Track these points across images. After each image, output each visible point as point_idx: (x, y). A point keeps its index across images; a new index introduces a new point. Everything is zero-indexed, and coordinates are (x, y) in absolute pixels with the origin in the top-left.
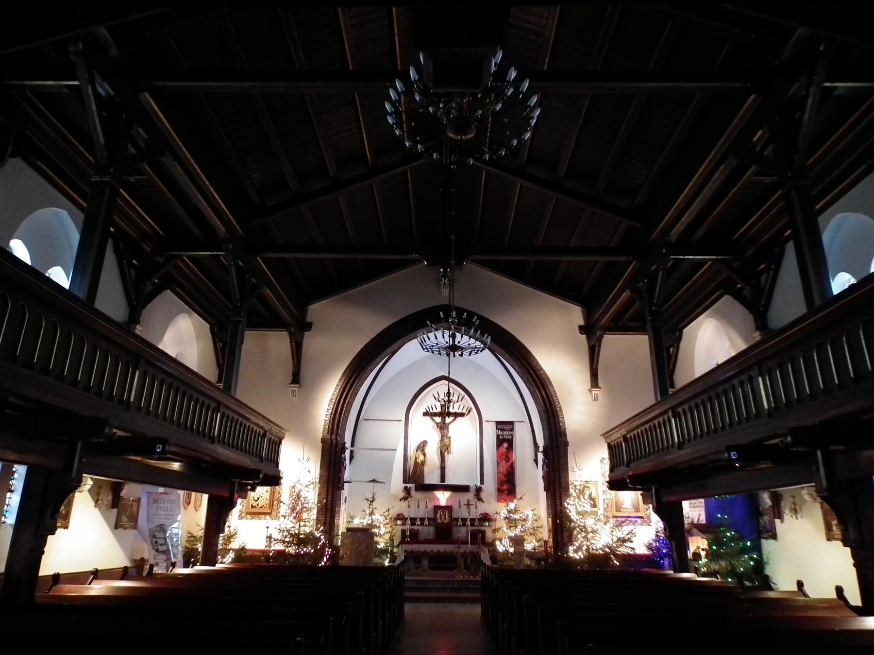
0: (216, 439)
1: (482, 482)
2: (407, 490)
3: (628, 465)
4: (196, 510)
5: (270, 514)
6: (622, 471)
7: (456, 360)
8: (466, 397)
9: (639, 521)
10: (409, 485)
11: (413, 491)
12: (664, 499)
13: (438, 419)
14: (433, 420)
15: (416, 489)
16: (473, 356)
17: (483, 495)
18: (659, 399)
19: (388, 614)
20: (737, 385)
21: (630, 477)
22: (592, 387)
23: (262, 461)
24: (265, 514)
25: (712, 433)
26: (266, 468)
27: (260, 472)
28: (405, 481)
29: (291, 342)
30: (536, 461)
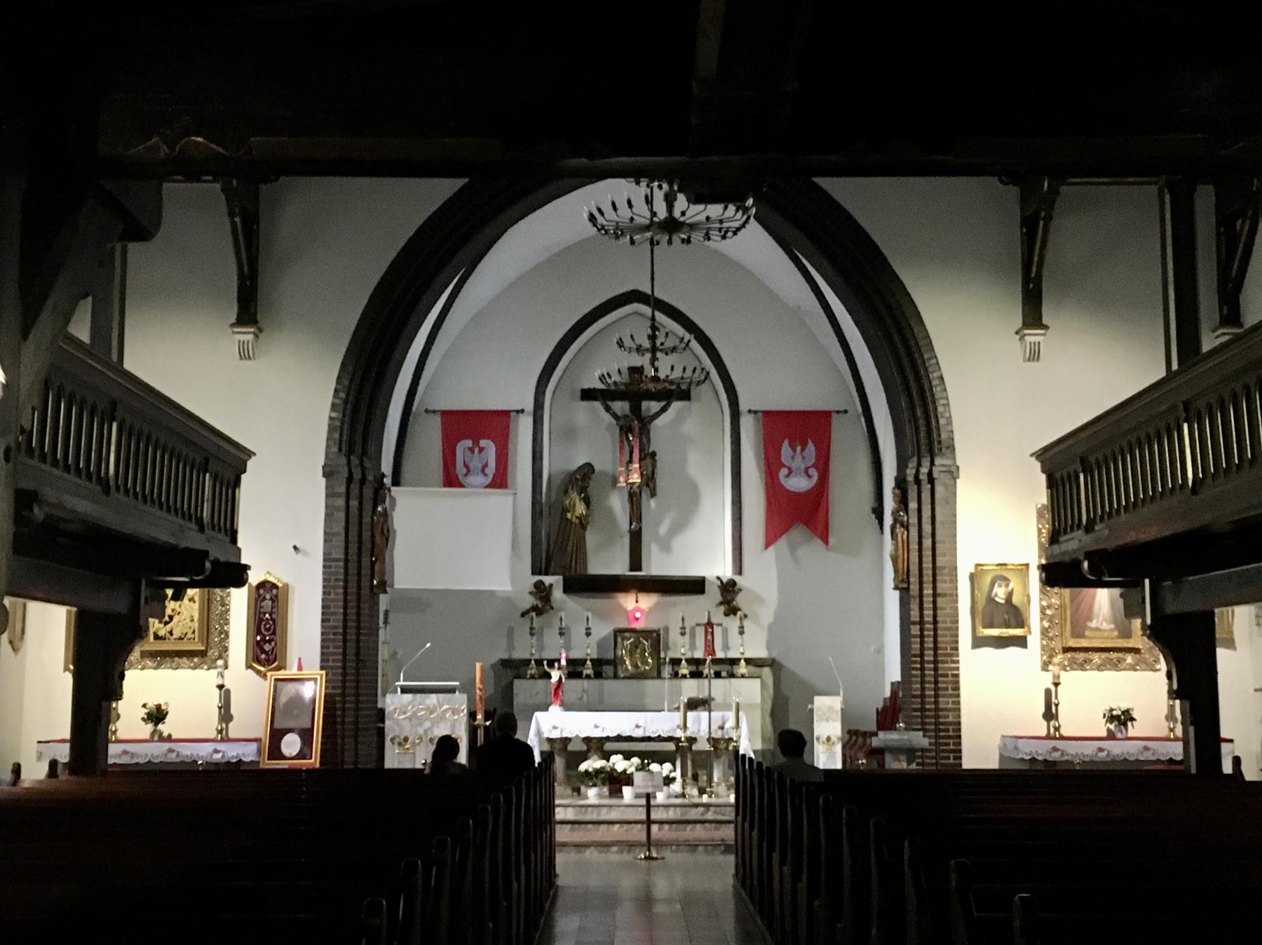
0: (112, 483)
1: (739, 569)
2: (542, 592)
3: (1089, 528)
4: (15, 649)
5: (203, 654)
6: (1074, 543)
7: (670, 252)
8: (695, 345)
9: (1129, 659)
10: (548, 580)
11: (558, 594)
12: (1172, 606)
13: (621, 407)
14: (608, 409)
15: (569, 588)
16: (716, 243)
17: (740, 600)
18: (1175, 366)
19: (515, 885)
20: (1227, 399)
21: (1089, 555)
22: (1026, 325)
23: (202, 529)
24: (190, 654)
25: (1140, 503)
26: (218, 552)
27: (205, 554)
28: (535, 572)
29: (231, 215)
30: (878, 512)
